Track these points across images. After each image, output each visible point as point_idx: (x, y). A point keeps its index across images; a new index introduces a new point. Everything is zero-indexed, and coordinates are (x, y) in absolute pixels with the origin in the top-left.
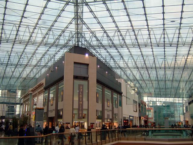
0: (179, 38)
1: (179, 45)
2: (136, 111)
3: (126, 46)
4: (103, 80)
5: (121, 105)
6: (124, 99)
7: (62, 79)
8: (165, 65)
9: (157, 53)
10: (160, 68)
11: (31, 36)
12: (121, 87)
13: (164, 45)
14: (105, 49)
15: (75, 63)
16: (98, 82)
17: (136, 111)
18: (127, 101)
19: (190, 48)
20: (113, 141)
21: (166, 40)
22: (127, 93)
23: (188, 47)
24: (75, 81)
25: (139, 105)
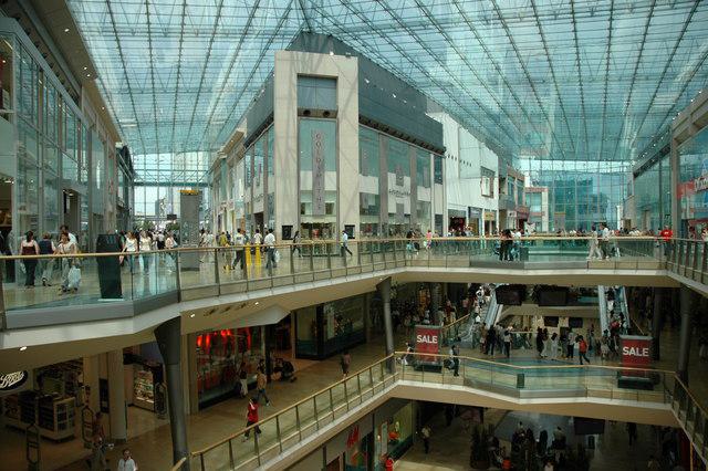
0: (184, 15)
1: (617, 12)
2: (489, 194)
3: (466, 21)
4: (375, 117)
5: (439, 179)
6: (450, 168)
7: (271, 119)
8: (607, 70)
9: (554, 37)
10: (165, 92)
11: (253, 17)
12: (442, 135)
13: (149, 32)
14: (412, 34)
15: (300, 76)
16: (364, 120)
17: (492, 195)
18: (460, 170)
19: (650, 16)
20: (219, 295)
21: (153, 19)
22: (460, 149)
23: (684, 10)
24: (303, 122)
25: (502, 181)
